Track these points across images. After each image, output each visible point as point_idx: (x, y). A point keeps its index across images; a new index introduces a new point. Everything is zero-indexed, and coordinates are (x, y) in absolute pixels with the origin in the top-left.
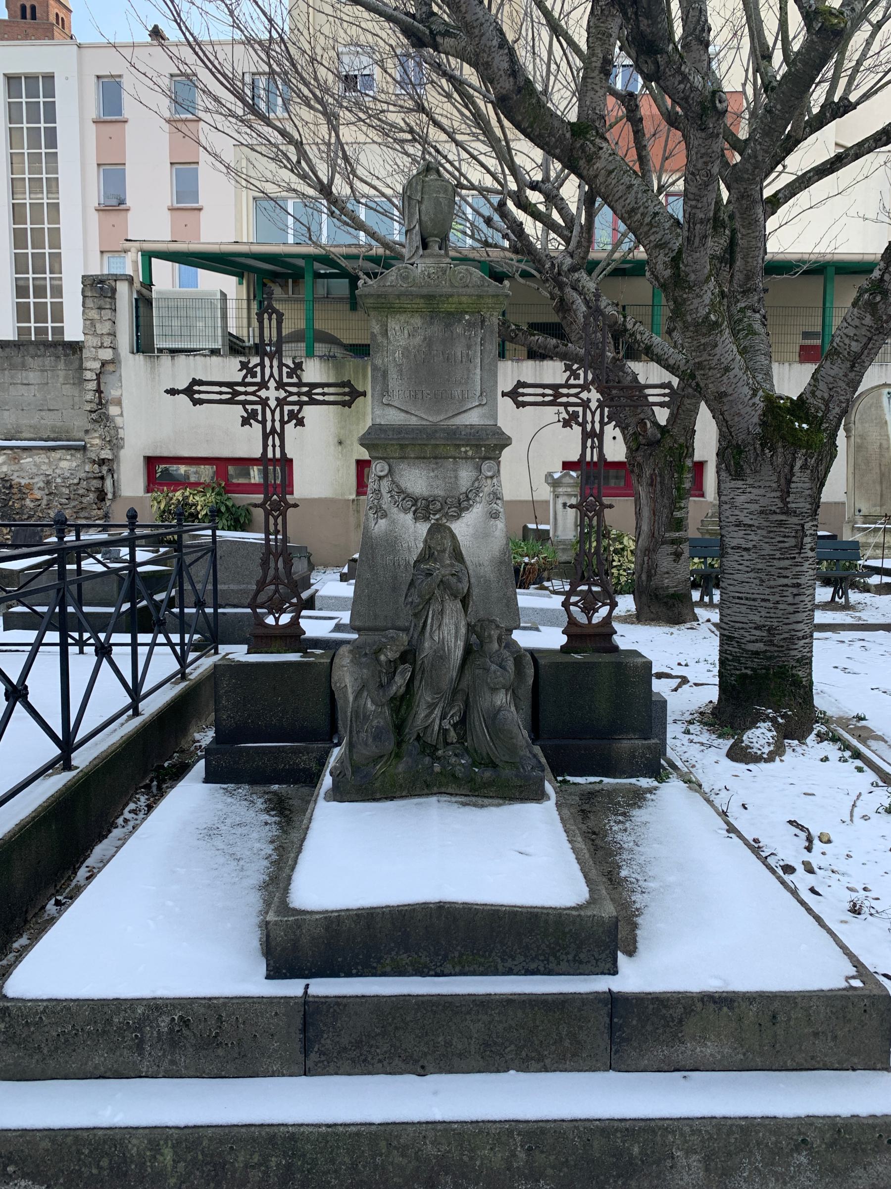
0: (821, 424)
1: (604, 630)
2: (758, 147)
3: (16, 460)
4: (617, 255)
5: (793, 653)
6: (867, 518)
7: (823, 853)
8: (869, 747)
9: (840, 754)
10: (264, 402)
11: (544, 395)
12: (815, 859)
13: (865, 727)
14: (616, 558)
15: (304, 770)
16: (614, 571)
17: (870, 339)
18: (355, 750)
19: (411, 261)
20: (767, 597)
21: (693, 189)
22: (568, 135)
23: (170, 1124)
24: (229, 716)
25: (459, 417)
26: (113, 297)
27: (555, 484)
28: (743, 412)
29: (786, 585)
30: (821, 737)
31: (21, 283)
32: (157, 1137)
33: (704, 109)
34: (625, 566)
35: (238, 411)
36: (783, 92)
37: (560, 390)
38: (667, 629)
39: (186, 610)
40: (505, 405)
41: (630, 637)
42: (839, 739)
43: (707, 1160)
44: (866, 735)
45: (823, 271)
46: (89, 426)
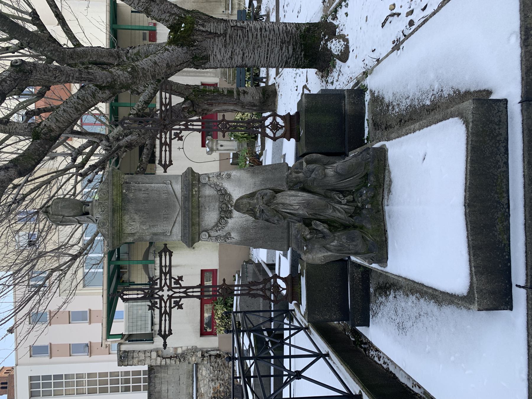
0: (182, 17)
1: (288, 119)
2: (47, 49)
4: (108, 123)
5: (294, 32)
6: (227, 9)
7: (401, 7)
9: (343, 7)
10: (170, 297)
11: (166, 151)
12: (404, 11)
15: (362, 275)
18: (359, 251)
19: (95, 221)
20: (267, 44)
22: (39, 141)
24: (334, 314)
25: (176, 193)
26: (128, 352)
27: (212, 150)
28: (176, 56)
29: (261, 35)
30: (335, 18)
31: (123, 389)
33: (20, 71)
35: (175, 311)
36: (19, 36)
37: (163, 142)
40: (171, 171)
42: (336, 9)
46: (187, 362)
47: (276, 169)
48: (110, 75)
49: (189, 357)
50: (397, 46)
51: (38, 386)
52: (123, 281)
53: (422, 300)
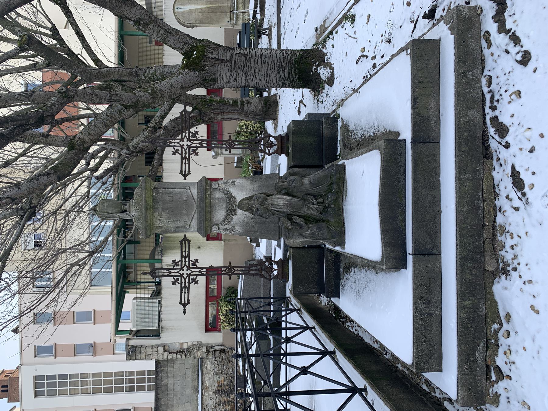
3: (207, 388)
5: (289, 58)
6: (232, 19)
8: (328, 27)
9: (331, 40)
11: (185, 163)
12: (371, 55)
13: (320, 28)
14: (249, 128)
16: (255, 129)
17: (159, 26)
21: (98, 100)
22: (74, 151)
23: (456, 302)
26: (136, 347)
27: (217, 154)
30: (324, 47)
31: (128, 389)
32: (460, 307)
33: (65, 96)
34: (253, 125)
35: (192, 286)
38: (280, 107)
39: (272, 309)
40: (189, 179)
41: (283, 128)
42: (325, 39)
43: (470, 109)
44: (323, 28)
45: (122, 36)
47: (270, 178)
48: (134, 96)
49: (194, 352)
50: (366, 80)
51: (43, 385)
52: (129, 281)
53: (368, 271)
